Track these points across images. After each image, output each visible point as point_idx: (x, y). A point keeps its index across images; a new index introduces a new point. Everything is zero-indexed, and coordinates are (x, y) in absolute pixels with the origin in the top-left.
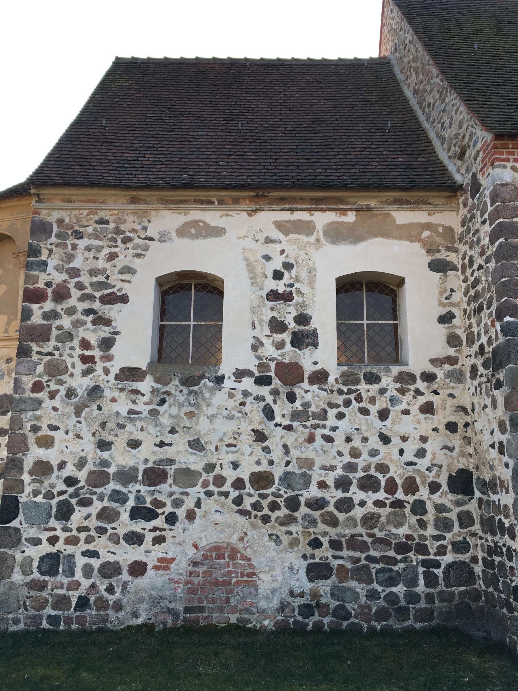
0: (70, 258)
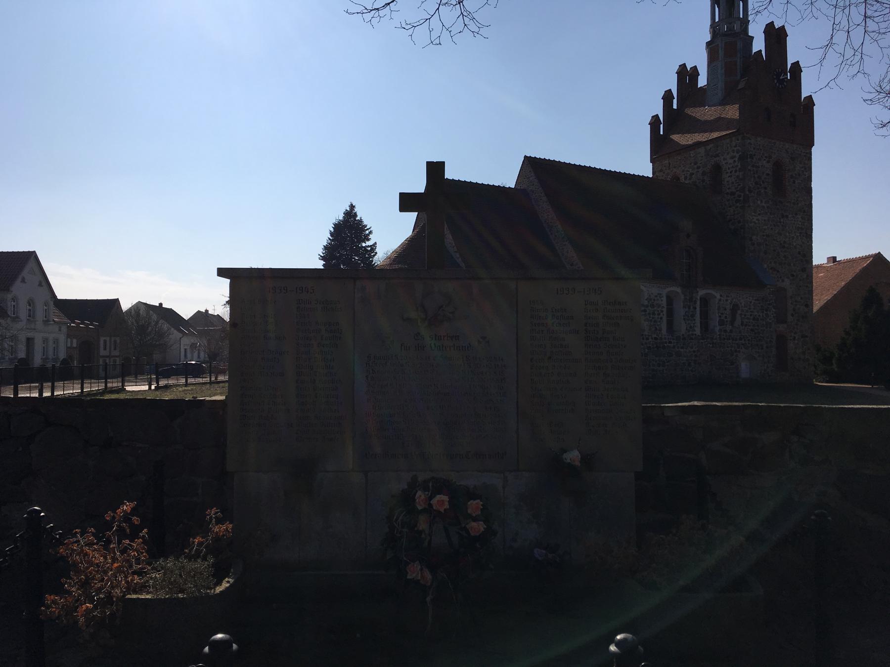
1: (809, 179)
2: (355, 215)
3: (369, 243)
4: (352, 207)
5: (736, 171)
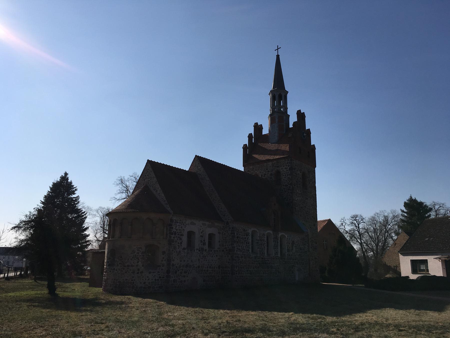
0: (176, 227)
1: (315, 182)
2: (68, 179)
3: (74, 196)
4: (66, 174)
5: (288, 175)
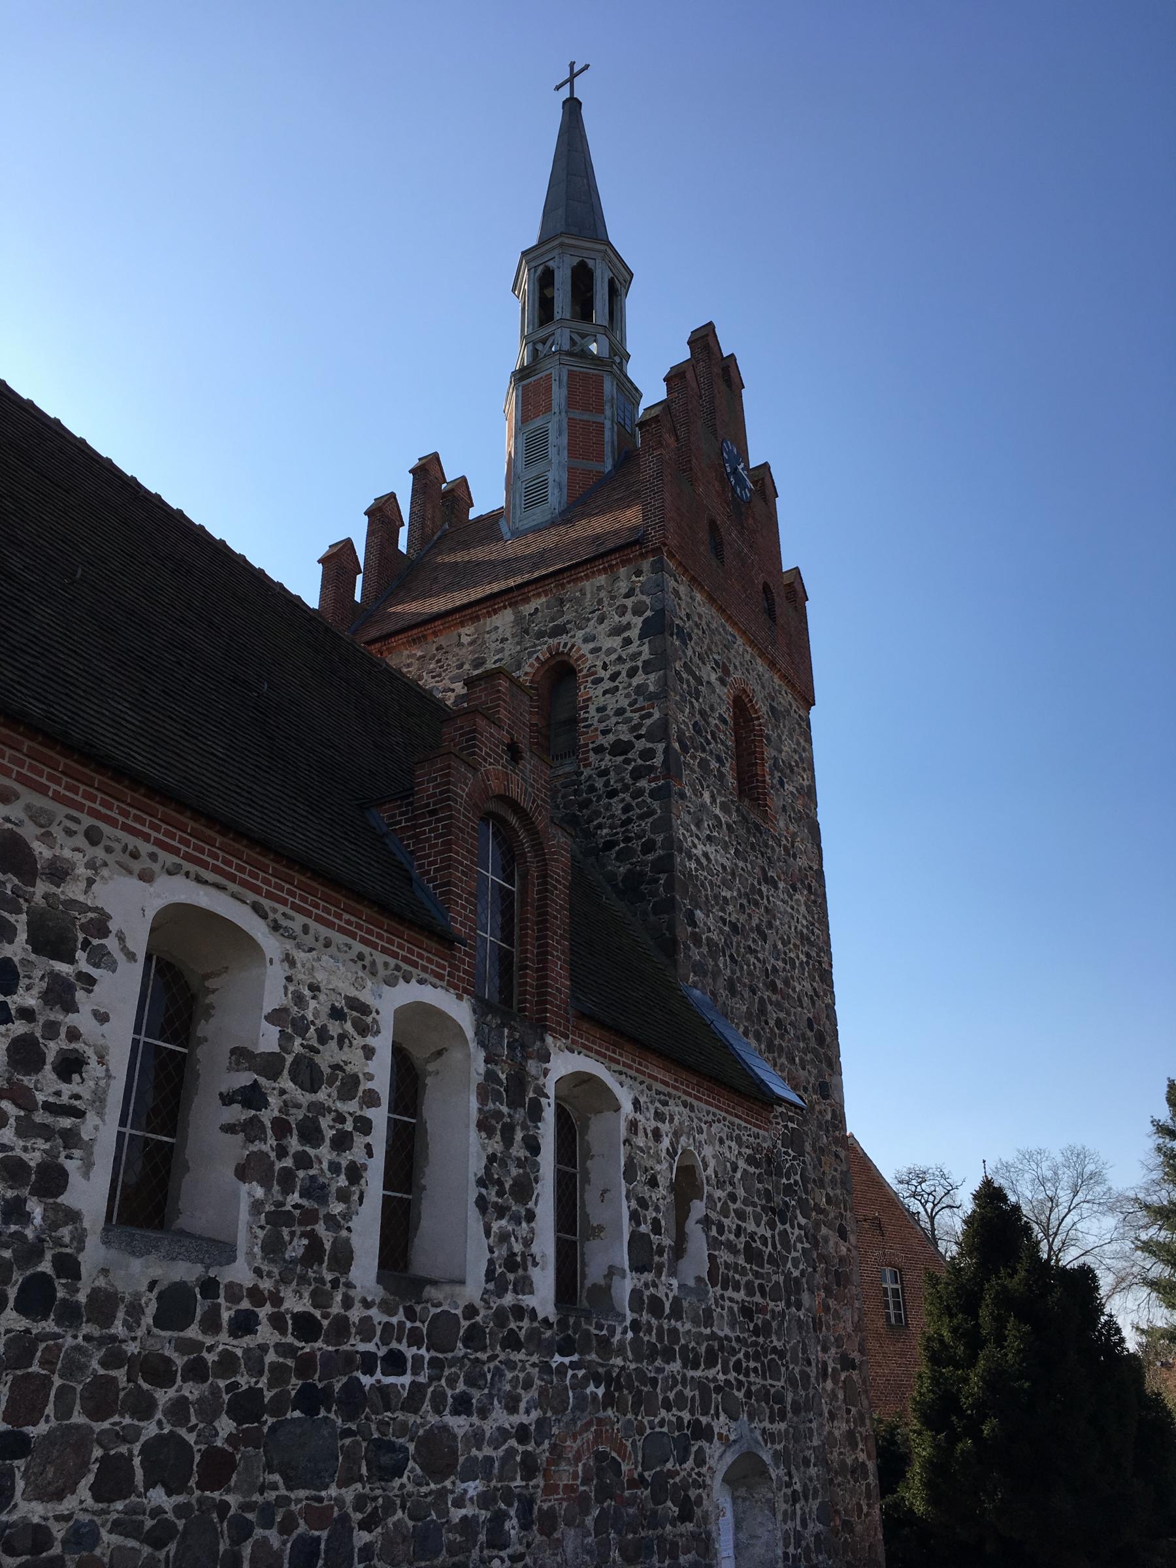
5: (632, 673)
